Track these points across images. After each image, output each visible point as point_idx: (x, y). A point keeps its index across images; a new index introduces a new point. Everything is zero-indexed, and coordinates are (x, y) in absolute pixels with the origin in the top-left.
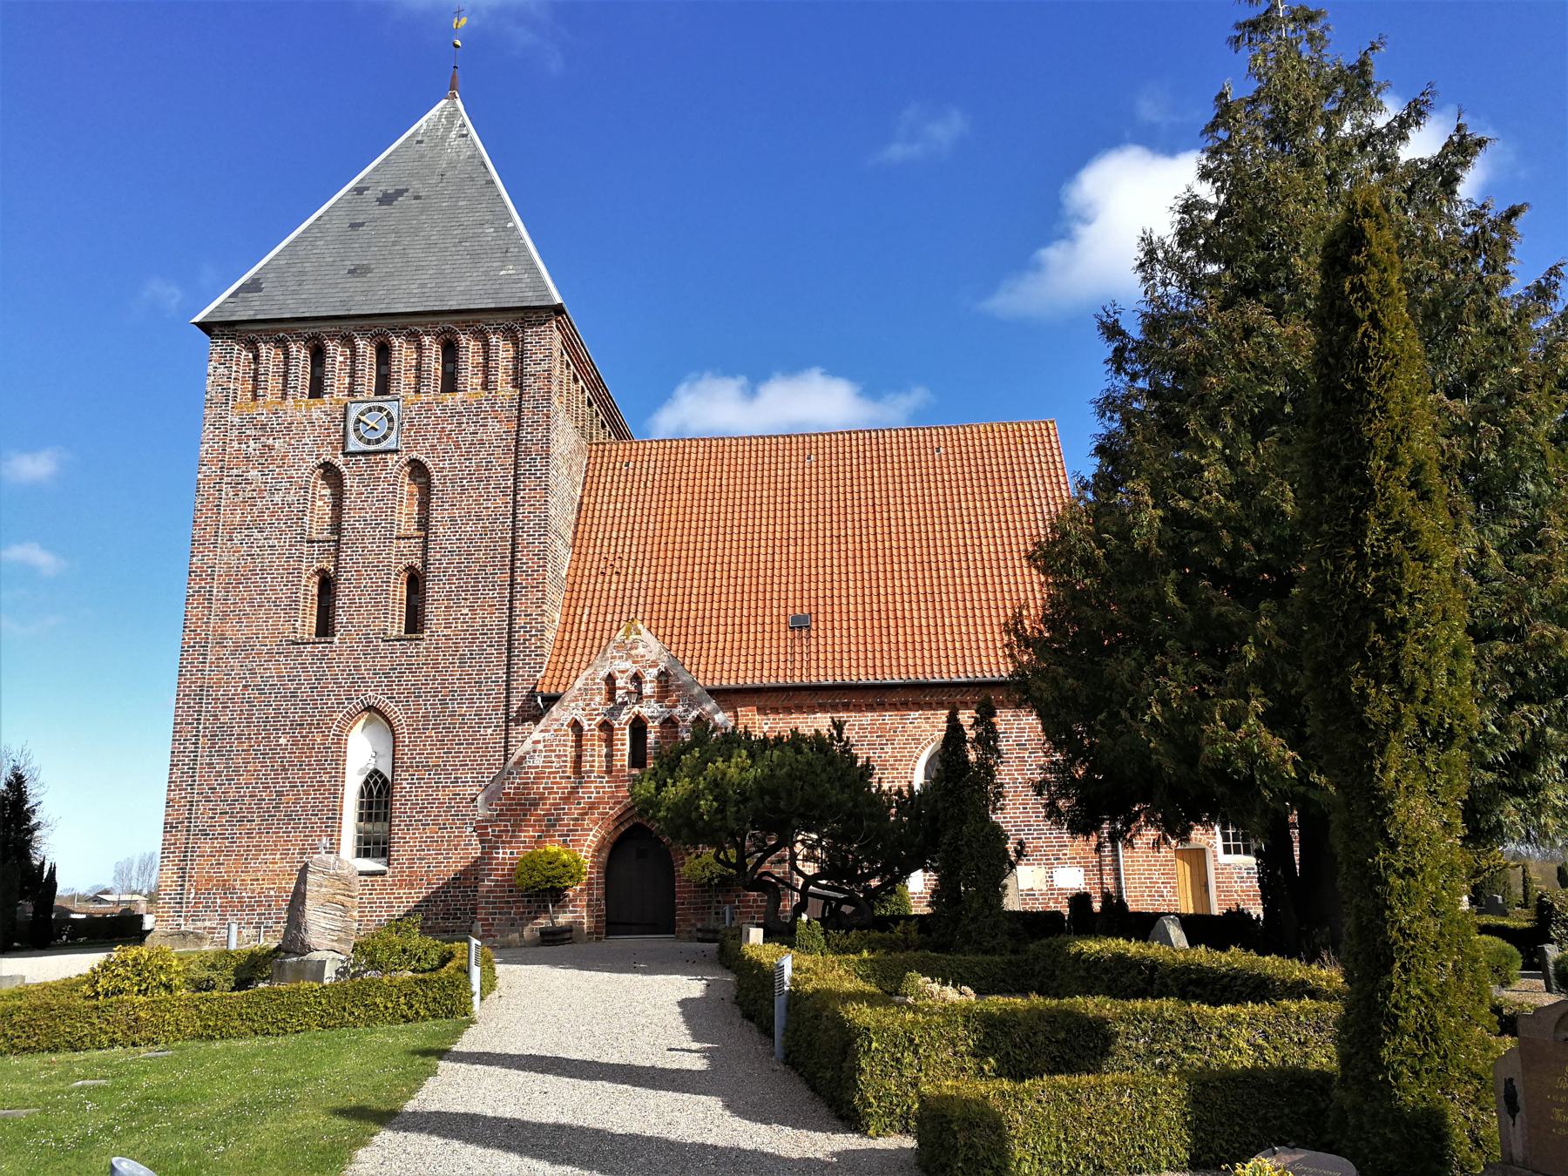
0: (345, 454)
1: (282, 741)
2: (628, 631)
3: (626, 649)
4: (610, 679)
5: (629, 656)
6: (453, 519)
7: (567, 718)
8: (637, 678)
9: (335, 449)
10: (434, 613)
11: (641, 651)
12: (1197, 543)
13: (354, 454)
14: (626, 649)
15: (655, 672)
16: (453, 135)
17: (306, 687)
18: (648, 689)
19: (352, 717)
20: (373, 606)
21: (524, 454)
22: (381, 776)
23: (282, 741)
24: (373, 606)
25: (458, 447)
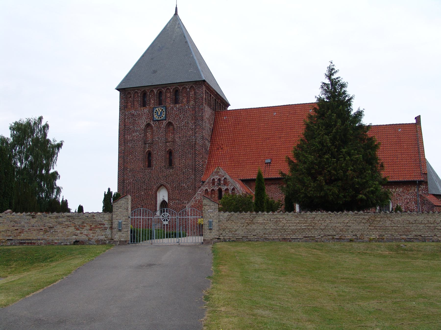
0: (153, 121)
1: (142, 193)
2: (217, 169)
3: (217, 173)
4: (214, 179)
5: (218, 175)
6: (180, 137)
7: (204, 189)
8: (219, 180)
9: (150, 120)
10: (176, 162)
11: (220, 173)
12: (42, 195)
13: (155, 121)
14: (217, 173)
15: (223, 178)
16: (176, 27)
17: (147, 180)
18: (222, 182)
19: (158, 188)
20: (159, 160)
21: (197, 118)
22: (166, 202)
23: (142, 193)
24: (159, 160)
25: (180, 118)
